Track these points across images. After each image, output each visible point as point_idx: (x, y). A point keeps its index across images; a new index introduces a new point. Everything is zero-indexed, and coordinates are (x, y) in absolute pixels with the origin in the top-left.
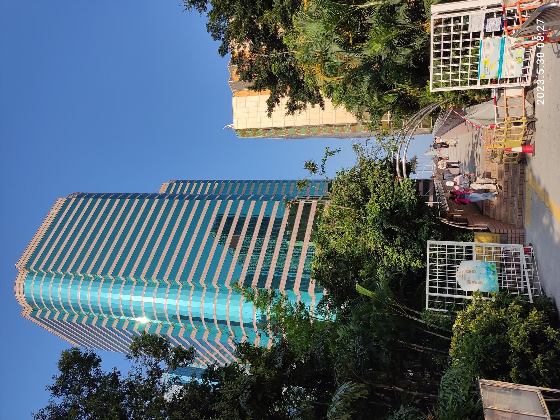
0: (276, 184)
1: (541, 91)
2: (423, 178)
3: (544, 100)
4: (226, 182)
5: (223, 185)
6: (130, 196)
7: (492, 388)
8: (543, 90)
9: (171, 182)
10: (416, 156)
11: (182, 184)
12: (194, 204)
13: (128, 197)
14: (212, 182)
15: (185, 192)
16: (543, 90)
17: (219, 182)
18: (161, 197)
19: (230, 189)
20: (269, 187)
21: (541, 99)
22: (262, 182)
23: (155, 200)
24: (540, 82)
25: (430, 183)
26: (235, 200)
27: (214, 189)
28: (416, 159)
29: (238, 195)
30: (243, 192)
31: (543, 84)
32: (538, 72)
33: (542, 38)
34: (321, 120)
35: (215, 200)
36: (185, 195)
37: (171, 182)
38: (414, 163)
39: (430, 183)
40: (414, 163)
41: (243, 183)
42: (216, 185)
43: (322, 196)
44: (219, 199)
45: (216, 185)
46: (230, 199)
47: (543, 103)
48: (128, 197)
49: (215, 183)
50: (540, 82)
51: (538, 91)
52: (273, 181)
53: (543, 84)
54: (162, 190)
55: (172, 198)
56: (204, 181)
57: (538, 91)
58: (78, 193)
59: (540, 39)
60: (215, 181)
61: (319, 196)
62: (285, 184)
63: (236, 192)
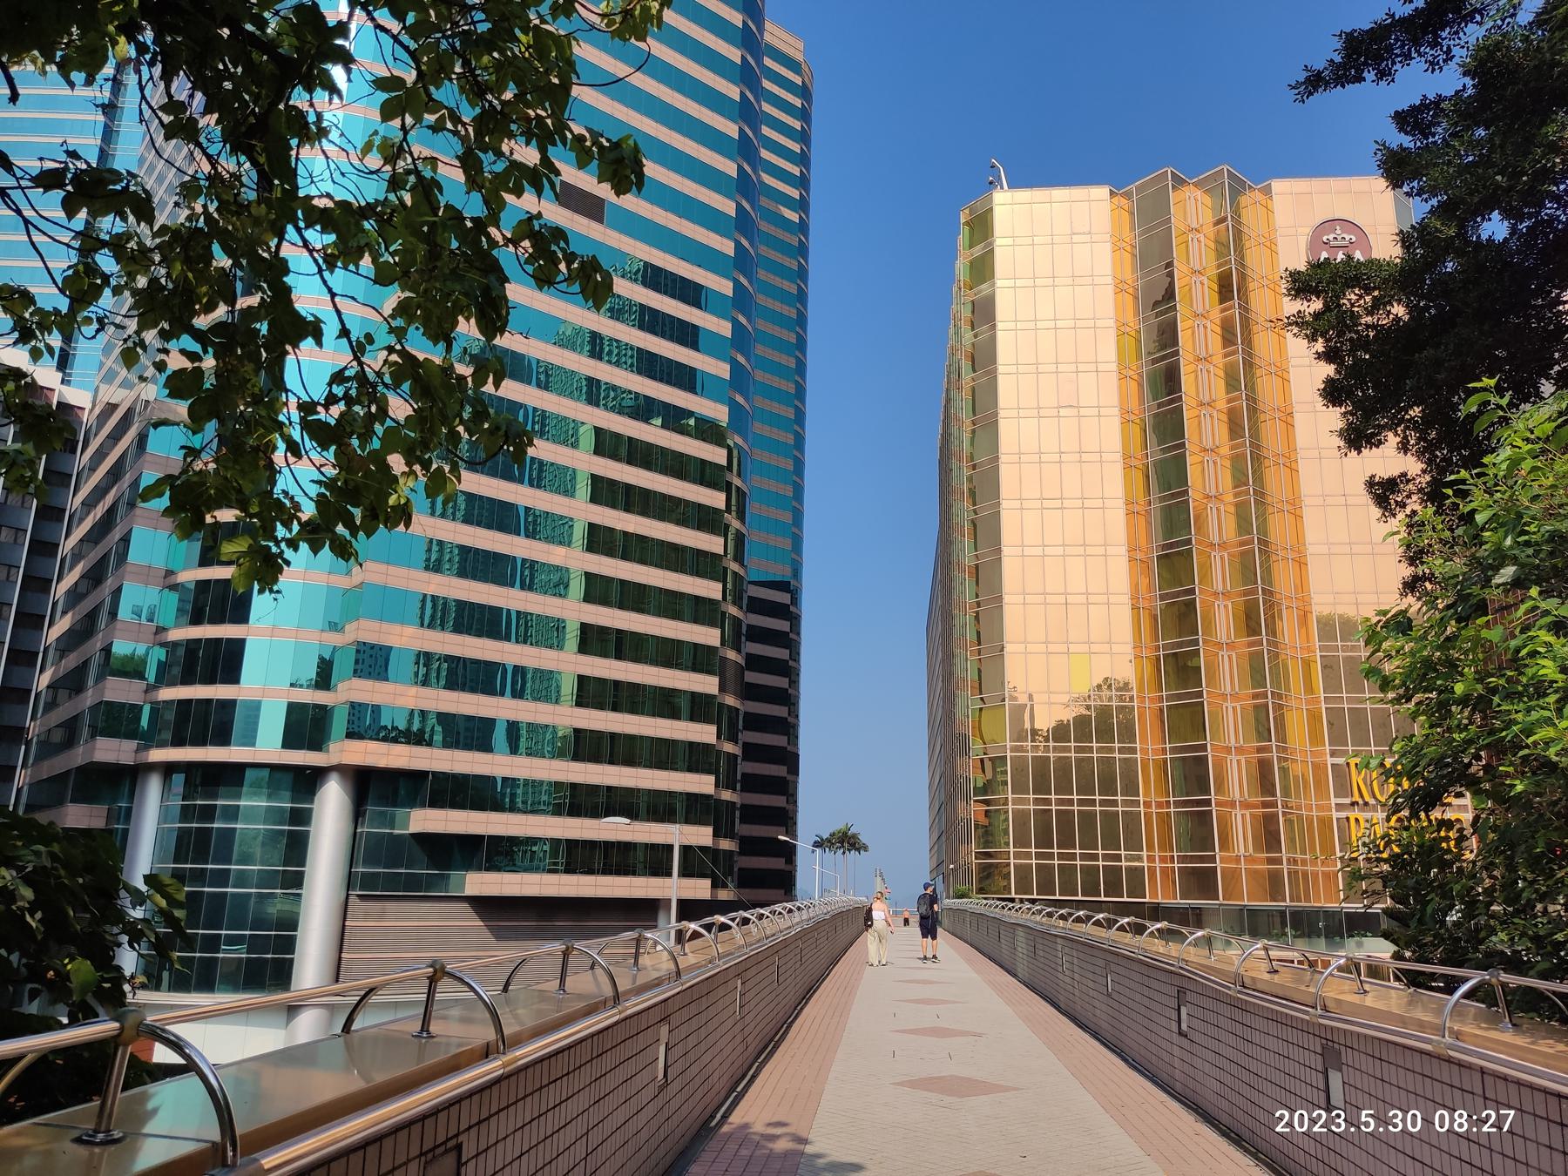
0: (792, 410)
1: (1313, 1121)
2: (798, 869)
3: (1288, 1130)
4: (803, 250)
5: (793, 237)
6: (753, 63)
7: (264, 1157)
8: (1316, 1129)
9: (807, 70)
10: (865, 848)
11: (796, 171)
12: (724, 77)
13: (750, 23)
14: (802, 205)
15: (766, 130)
16: (1316, 1129)
17: (803, 227)
18: (749, 40)
19: (780, 261)
20: (784, 388)
21: (1290, 1124)
22: (800, 417)
23: (736, 122)
24: (1337, 1121)
25: (783, 892)
26: (735, 266)
27: (781, 207)
28: (858, 850)
29: (750, 436)
30: (762, 300)
31: (1390, 1128)
32: (1367, 1116)
33: (1461, 1125)
34: (1017, 504)
35: (733, 353)
36: (756, 131)
37: (807, 70)
38: (846, 845)
39: (783, 892)
40: (846, 845)
41: (798, 329)
42: (793, 216)
43: (744, 530)
44: (738, 286)
45: (793, 216)
46: (736, 325)
47: (1278, 1129)
48: (750, 23)
49: (799, 286)
50: (1337, 1121)
51: (1314, 1115)
52: (802, 427)
53: (1390, 1128)
54: (774, 34)
55: (747, 76)
56: (807, 249)
57: (1314, 1115)
58: (763, 6)
59: (1463, 1121)
60: (807, 262)
61: (742, 564)
62: (787, 517)
63: (760, 350)
